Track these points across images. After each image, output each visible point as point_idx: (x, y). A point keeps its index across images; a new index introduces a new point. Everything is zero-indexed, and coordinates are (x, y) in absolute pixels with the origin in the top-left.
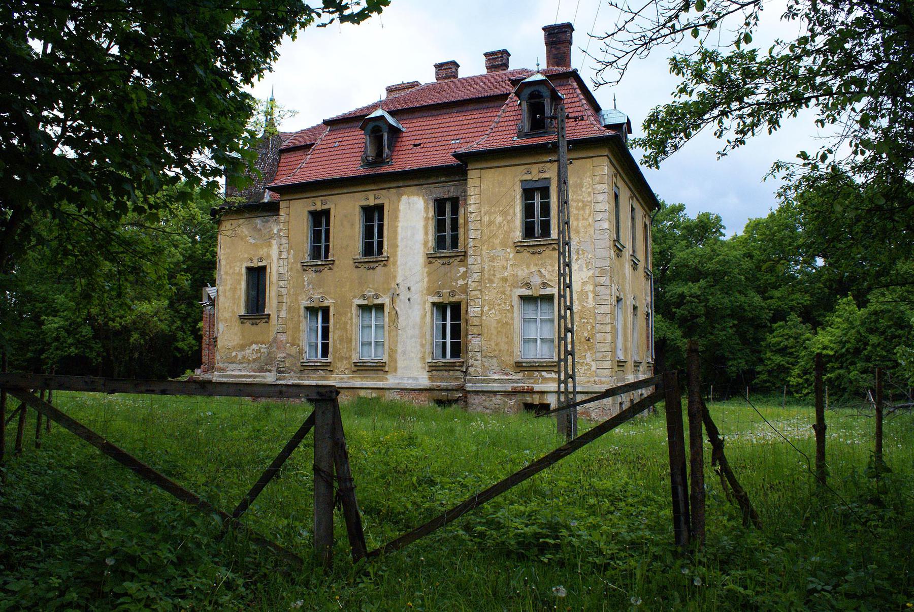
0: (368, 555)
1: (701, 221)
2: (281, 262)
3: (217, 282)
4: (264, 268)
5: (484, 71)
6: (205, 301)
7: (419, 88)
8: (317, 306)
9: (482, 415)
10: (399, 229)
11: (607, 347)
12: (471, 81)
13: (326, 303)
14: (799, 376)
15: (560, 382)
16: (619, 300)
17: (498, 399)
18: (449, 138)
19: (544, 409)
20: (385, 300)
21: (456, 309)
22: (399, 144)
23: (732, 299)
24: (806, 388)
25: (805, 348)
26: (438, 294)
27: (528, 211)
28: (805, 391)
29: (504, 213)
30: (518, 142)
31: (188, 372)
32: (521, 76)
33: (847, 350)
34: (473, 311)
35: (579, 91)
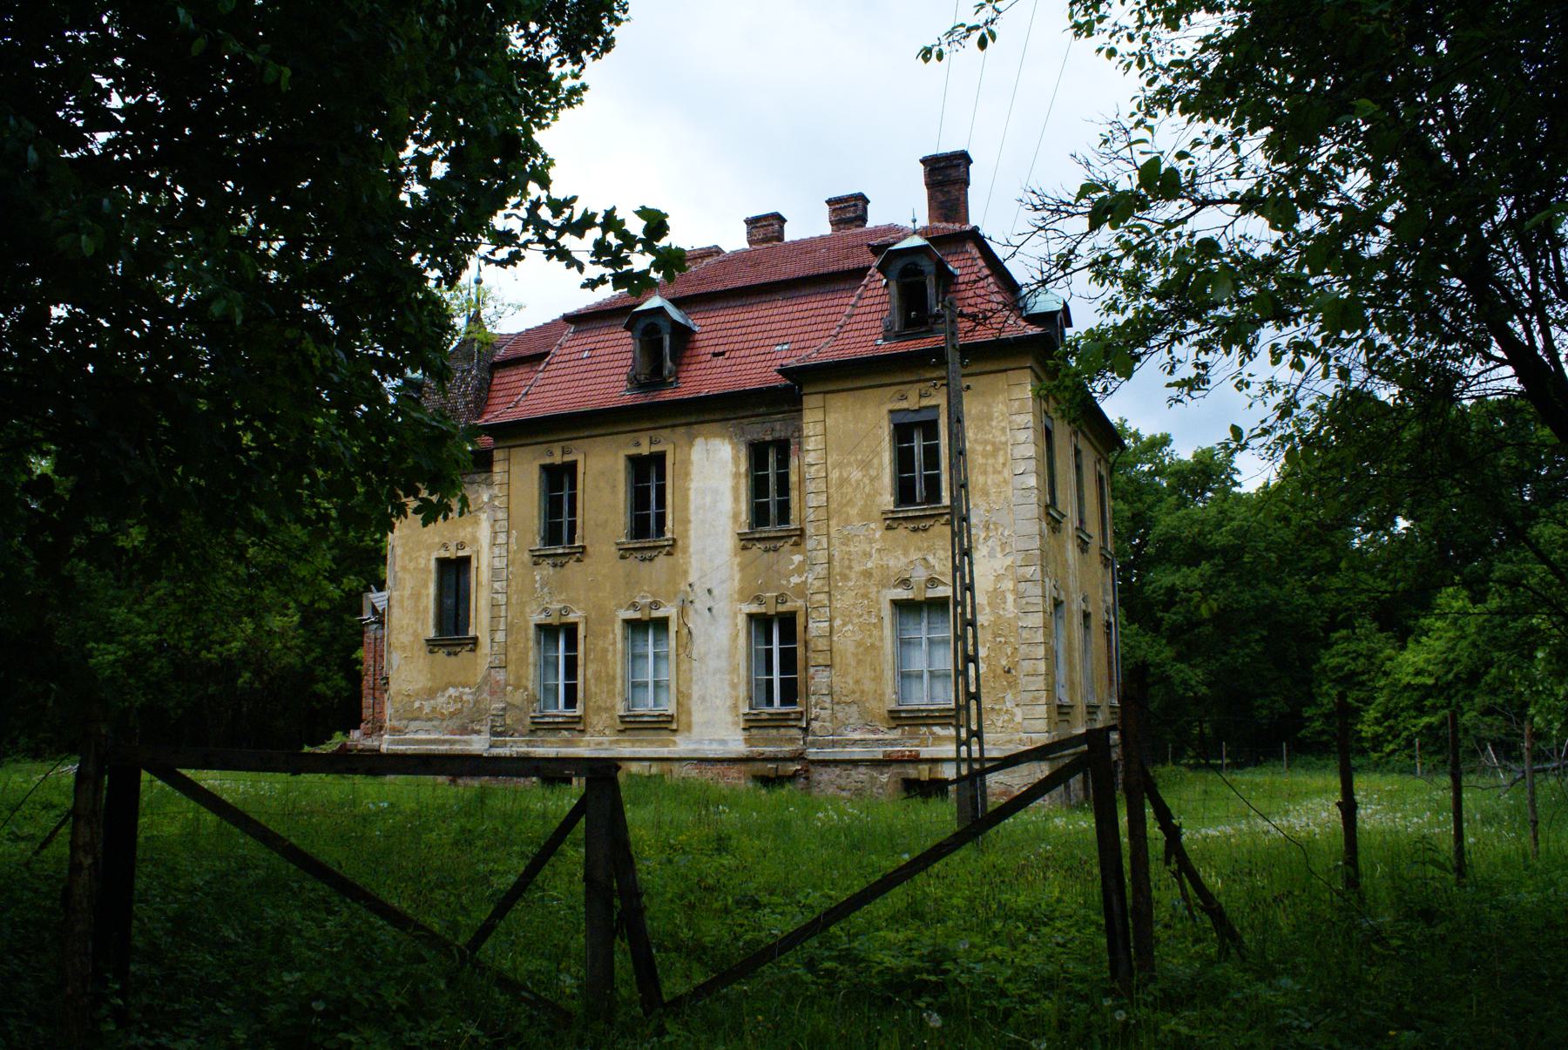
0: (665, 1006)
1: (1199, 462)
2: (497, 550)
3: (389, 583)
4: (467, 560)
5: (826, 229)
6: (367, 615)
7: (721, 258)
8: (556, 622)
9: (833, 800)
10: (692, 494)
11: (1040, 683)
12: (806, 247)
13: (571, 618)
14: (1378, 722)
15: (959, 743)
16: (1058, 604)
17: (861, 774)
18: (772, 341)
19: (936, 787)
20: (669, 611)
21: (788, 623)
22: (688, 353)
23: (1257, 593)
24: (1390, 742)
25: (1386, 674)
26: (758, 599)
27: (903, 460)
28: (1388, 748)
29: (865, 465)
30: (885, 347)
31: (338, 738)
32: (889, 238)
33: (1457, 676)
34: (817, 627)
35: (981, 263)
